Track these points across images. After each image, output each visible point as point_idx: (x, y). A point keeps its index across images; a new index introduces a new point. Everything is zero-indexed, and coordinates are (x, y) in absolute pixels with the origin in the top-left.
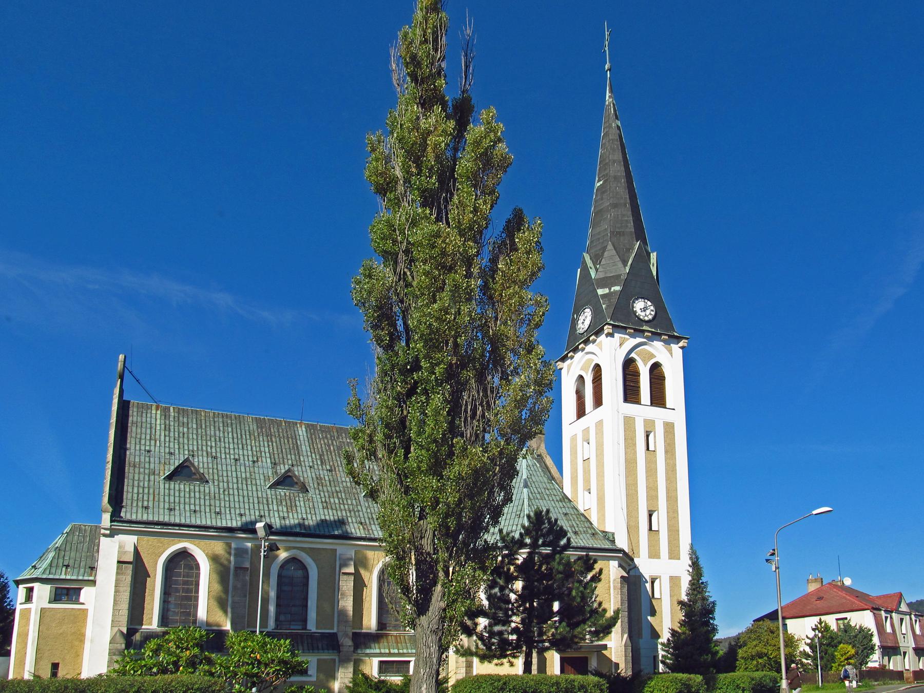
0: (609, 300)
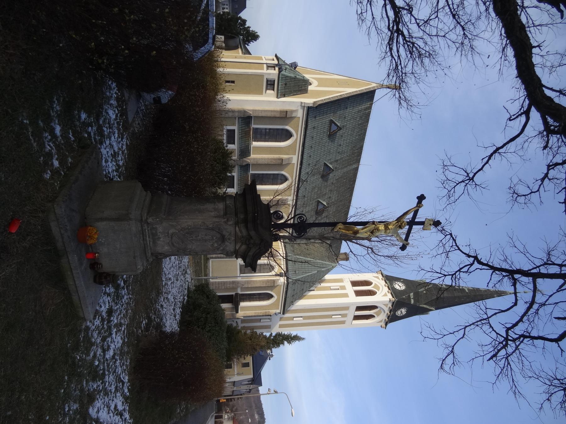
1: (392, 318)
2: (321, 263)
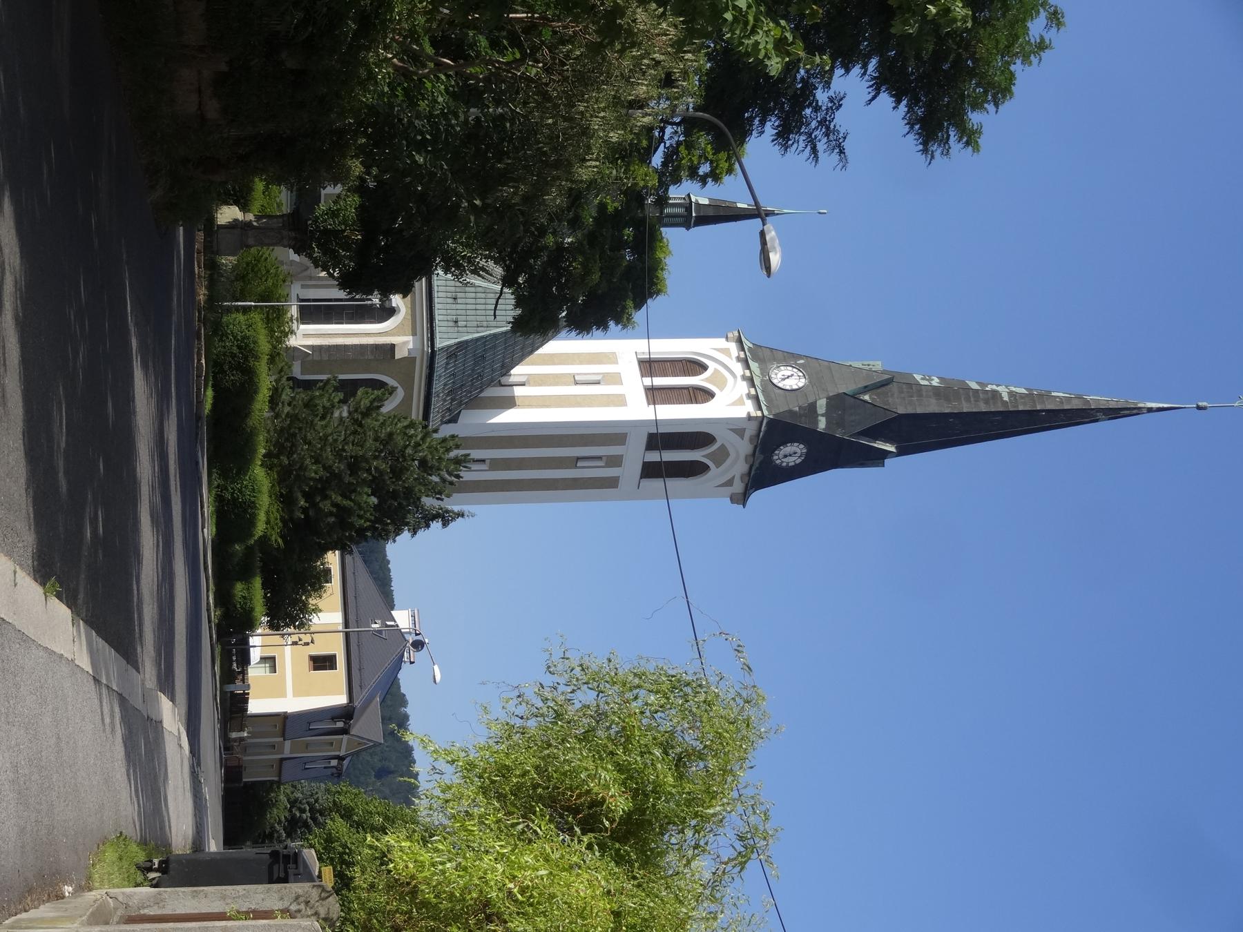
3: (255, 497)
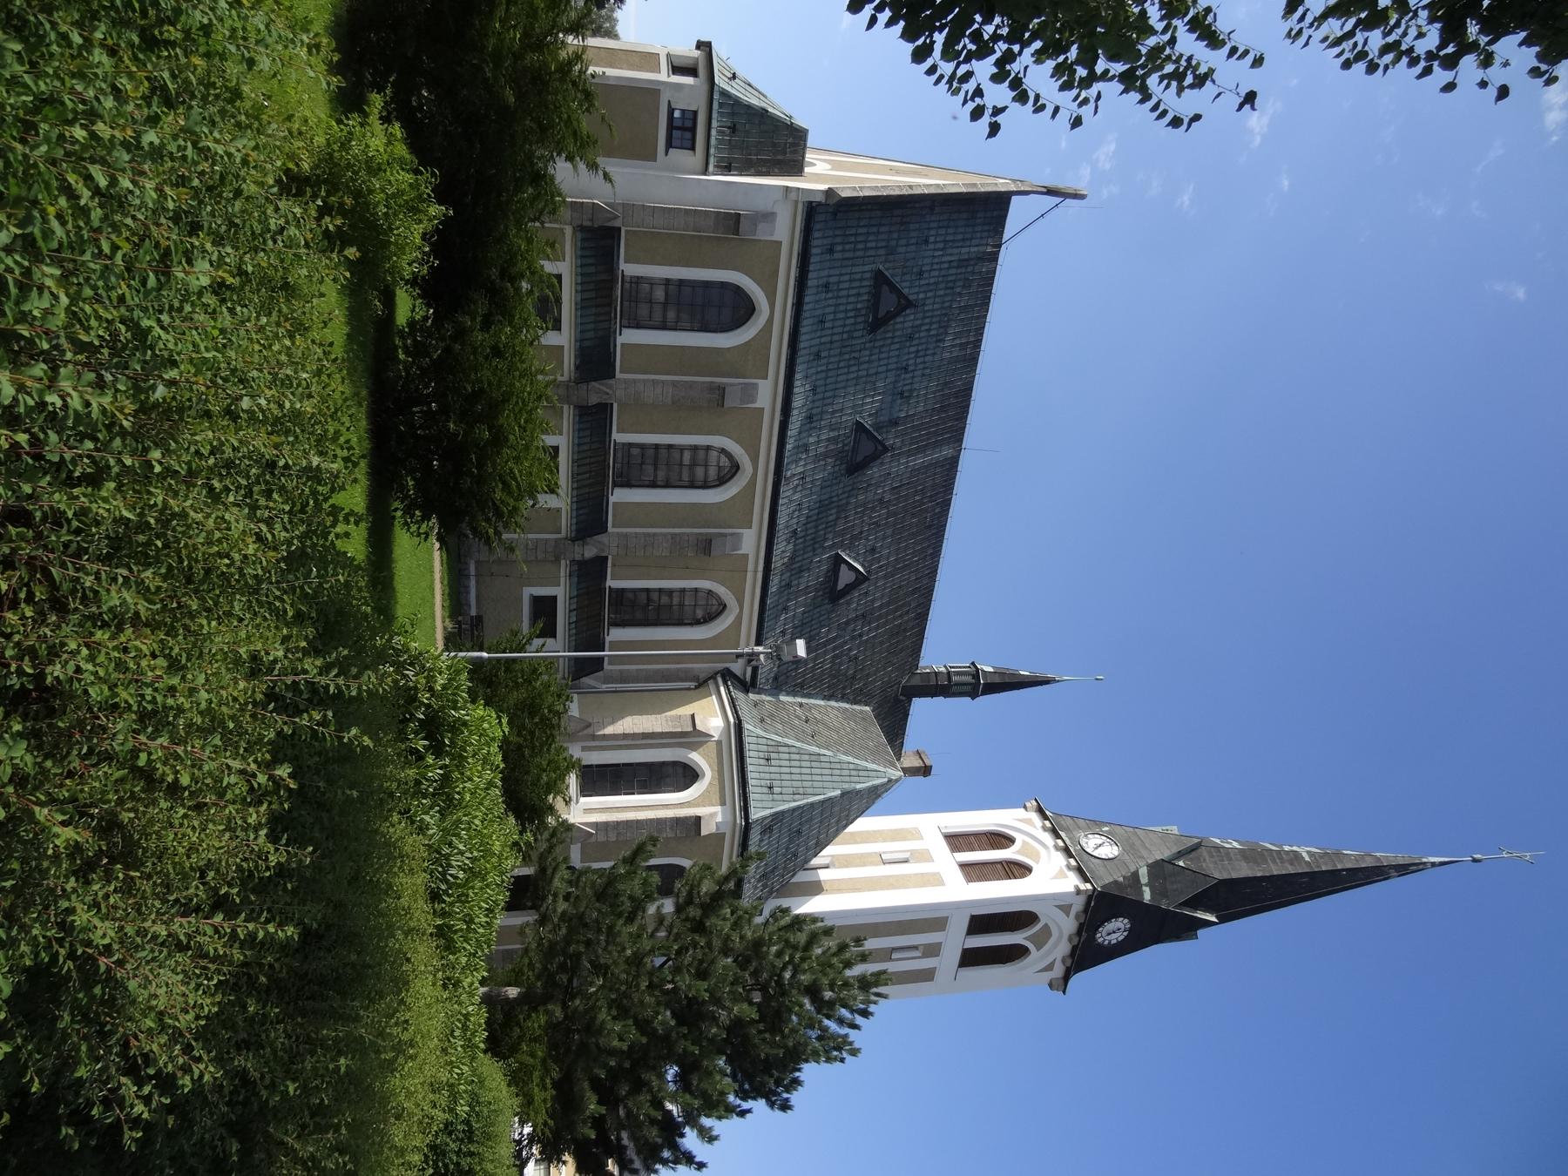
0: (1129, 886)
1: (1086, 954)
2: (851, 766)
3: (471, 1154)
